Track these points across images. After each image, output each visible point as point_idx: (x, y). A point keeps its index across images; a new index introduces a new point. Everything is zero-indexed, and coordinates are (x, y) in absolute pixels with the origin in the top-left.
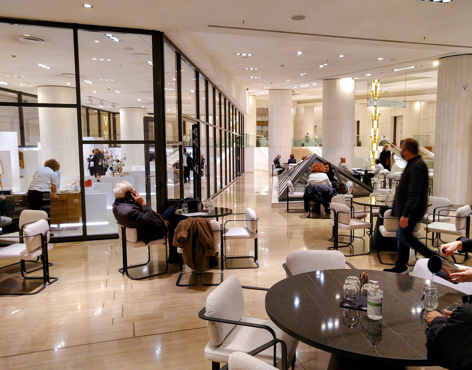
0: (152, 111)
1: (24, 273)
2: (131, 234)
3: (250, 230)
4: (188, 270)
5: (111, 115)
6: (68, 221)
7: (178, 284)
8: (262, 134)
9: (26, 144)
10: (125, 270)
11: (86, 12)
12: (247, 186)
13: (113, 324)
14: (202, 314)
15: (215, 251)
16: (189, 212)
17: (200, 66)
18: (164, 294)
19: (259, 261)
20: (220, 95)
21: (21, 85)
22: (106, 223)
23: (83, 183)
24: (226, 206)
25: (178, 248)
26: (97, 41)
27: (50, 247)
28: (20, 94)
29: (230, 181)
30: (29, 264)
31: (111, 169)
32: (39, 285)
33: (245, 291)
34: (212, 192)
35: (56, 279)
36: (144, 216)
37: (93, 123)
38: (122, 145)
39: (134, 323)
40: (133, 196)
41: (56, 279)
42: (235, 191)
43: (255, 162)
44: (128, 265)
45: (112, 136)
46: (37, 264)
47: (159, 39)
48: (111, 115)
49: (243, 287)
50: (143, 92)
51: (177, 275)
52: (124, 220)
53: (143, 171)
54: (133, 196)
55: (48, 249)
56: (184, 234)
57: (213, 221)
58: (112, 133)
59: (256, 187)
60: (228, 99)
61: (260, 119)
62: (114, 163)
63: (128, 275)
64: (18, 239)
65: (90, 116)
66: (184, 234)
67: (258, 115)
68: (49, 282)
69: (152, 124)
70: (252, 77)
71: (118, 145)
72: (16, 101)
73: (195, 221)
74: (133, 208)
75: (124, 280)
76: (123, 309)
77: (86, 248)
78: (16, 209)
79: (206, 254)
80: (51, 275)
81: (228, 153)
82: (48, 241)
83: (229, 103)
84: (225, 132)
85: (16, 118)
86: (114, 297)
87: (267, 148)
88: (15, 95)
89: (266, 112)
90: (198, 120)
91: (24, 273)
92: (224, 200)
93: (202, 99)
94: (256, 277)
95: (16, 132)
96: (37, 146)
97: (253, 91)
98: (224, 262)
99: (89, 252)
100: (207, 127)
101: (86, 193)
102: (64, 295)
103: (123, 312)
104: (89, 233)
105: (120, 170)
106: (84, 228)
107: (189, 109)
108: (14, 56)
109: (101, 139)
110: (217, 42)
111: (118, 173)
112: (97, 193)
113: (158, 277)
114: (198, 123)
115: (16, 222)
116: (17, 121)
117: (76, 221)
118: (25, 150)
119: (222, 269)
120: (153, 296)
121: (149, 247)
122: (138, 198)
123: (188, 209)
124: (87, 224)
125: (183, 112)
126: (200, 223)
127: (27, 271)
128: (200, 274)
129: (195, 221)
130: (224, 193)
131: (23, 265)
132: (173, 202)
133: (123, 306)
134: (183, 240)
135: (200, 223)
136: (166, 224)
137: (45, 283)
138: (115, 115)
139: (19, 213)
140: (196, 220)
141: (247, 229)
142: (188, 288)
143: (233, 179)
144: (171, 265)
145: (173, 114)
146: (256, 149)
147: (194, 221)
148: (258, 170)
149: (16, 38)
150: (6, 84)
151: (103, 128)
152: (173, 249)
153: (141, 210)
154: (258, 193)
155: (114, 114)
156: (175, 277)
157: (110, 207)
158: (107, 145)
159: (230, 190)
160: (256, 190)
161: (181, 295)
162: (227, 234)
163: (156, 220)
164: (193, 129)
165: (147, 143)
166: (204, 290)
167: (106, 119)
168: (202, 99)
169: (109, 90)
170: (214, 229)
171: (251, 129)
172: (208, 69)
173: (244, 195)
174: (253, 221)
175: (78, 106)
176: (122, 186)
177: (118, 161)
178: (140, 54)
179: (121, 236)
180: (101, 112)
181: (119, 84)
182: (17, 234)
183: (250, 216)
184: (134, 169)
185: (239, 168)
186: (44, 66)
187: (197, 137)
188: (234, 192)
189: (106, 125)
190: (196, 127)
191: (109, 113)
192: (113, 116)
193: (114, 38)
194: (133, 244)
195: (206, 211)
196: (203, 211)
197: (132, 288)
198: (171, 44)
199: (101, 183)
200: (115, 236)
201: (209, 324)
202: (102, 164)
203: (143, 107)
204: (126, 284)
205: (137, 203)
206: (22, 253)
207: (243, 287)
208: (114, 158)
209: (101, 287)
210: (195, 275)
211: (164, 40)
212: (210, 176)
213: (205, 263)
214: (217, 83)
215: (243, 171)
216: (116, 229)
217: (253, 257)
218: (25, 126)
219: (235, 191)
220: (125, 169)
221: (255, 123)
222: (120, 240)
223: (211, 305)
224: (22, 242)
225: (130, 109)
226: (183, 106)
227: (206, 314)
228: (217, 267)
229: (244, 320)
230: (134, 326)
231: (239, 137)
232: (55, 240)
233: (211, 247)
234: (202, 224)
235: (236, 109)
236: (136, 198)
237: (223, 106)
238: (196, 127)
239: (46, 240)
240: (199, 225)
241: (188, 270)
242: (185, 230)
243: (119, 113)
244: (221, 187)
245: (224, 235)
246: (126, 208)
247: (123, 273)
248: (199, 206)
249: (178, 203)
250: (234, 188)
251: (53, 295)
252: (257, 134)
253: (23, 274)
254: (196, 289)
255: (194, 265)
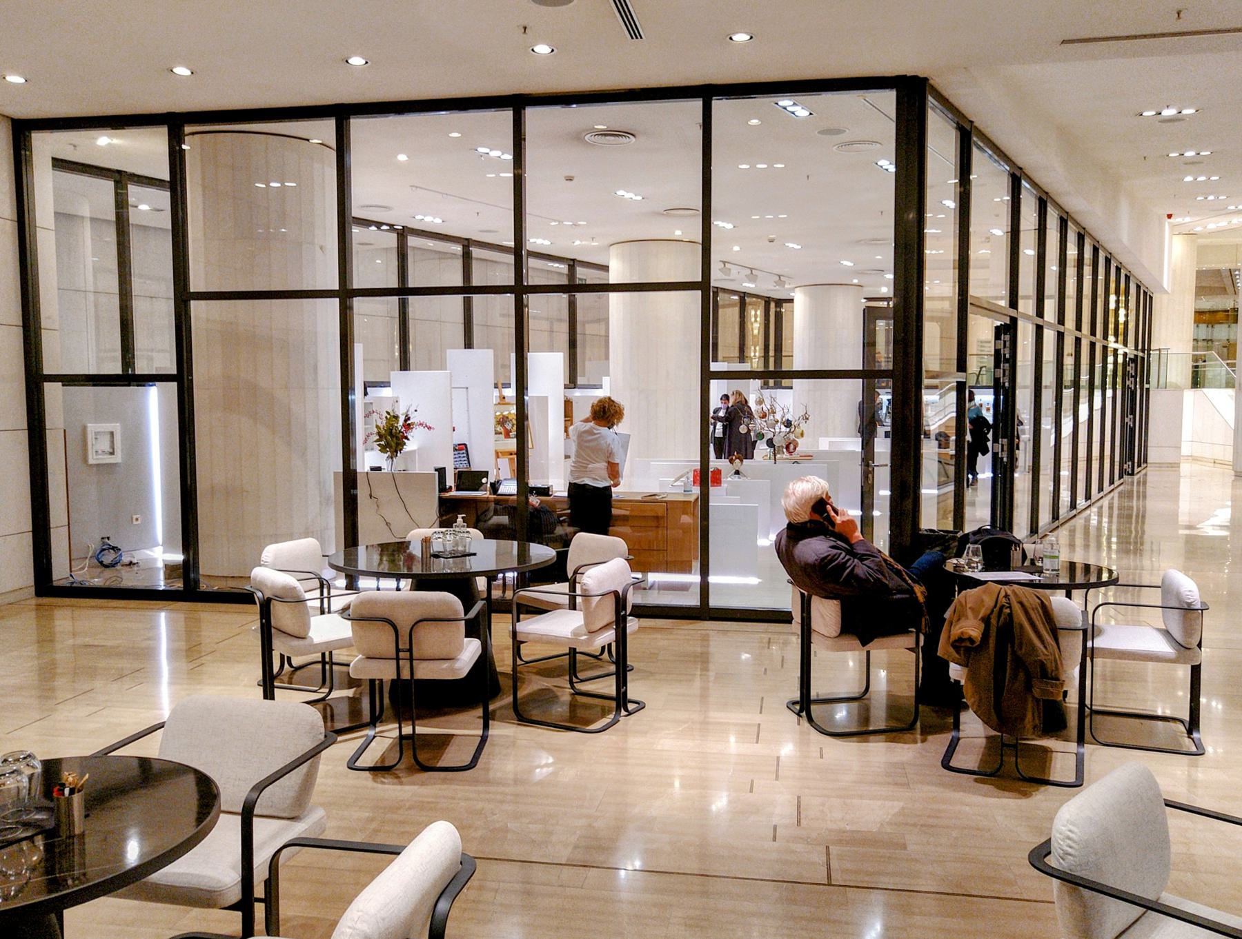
0: (886, 290)
1: (575, 680)
2: (826, 614)
3: (1177, 634)
4: (973, 727)
5: (773, 305)
6: (668, 567)
7: (946, 764)
8: (1209, 349)
9: (580, 381)
10: (804, 705)
11: (357, 76)
12: (1154, 505)
13: (774, 840)
14: (1039, 856)
15: (1062, 685)
16: (987, 568)
17: (1028, 157)
18: (907, 785)
19: (1203, 735)
20: (1081, 238)
21: (577, 243)
22: (754, 581)
23: (706, 478)
24: (1099, 559)
25: (952, 665)
26: (754, 122)
27: (633, 624)
28: (572, 264)
29: (1101, 489)
30: (584, 662)
31: (770, 443)
32: (604, 713)
33: (1176, 820)
34: (1045, 517)
35: (641, 706)
36: (861, 569)
37: (736, 330)
38: (796, 382)
39: (827, 848)
40: (832, 513)
41: (641, 706)
42: (1115, 519)
43: (1186, 434)
44: (813, 695)
45: (772, 360)
46: (599, 663)
47: (912, 95)
48: (773, 305)
49: (1169, 804)
50: (858, 242)
51: (947, 737)
52: (813, 578)
53: (853, 452)
54: (832, 513)
55: (628, 631)
56: (972, 628)
57: (1057, 599)
58: (772, 353)
59: (1185, 508)
60: (1105, 250)
61: (1207, 304)
62: (777, 430)
63: (810, 720)
64: (565, 600)
65: (720, 311)
66: (972, 628)
67: (1201, 291)
68: (626, 710)
69: (883, 328)
70: (1189, 179)
71: (785, 382)
72: (564, 281)
73: (1006, 596)
74: (833, 547)
75: (802, 733)
76: (799, 807)
77: (705, 639)
78: (560, 531)
79: (1036, 692)
80: (630, 696)
81: (1097, 408)
82: (629, 610)
83: (1108, 261)
84: (1093, 345)
85: (560, 320)
86: (777, 771)
87: (1231, 392)
88: (563, 268)
89: (1228, 281)
90: (1012, 312)
91: (575, 680)
92: (1079, 541)
93: (1028, 252)
94: (1192, 783)
95: (561, 354)
96: (600, 387)
97: (1187, 219)
98: (1087, 721)
99: (712, 649)
100: (1039, 330)
101: (712, 503)
102: (659, 747)
103: (799, 813)
104: (714, 602)
105: (792, 447)
106: (705, 588)
107: (988, 281)
108: (570, 179)
109: (745, 367)
110: (1073, 83)
111: (786, 455)
112: (733, 502)
113: (882, 737)
114: (1014, 321)
115: (562, 557)
116: (565, 327)
117: (685, 568)
118: (577, 393)
119: (1081, 741)
120: (875, 787)
121: (868, 653)
122: (845, 519)
123: (984, 558)
124: (712, 579)
125: (974, 291)
126: (1021, 603)
127: (581, 675)
128: (1015, 746)
129: (1006, 596)
130: (1079, 522)
131: (572, 662)
132: (934, 538)
133: (799, 797)
134: (968, 644)
135: (1021, 603)
136: (919, 594)
137: (618, 709)
138: (781, 307)
139: (566, 542)
140: (1009, 592)
141: (1167, 633)
142: (976, 780)
143: (1112, 482)
144: (932, 706)
145: (942, 299)
146: (1190, 395)
147: (1003, 593)
148: (1195, 459)
149: (578, 138)
150: (547, 243)
151: (749, 340)
152: (932, 669)
153: (851, 552)
154: (1190, 527)
155: (779, 303)
156: (939, 743)
157: (767, 540)
158: (758, 382)
159: (1098, 516)
160: (1183, 519)
161: (958, 795)
162: (1099, 643)
163: (892, 581)
164: (997, 337)
165: (869, 375)
166: (1025, 795)
167: (756, 316)
168: (1028, 252)
169: (771, 241)
170: (1061, 623)
171: (1174, 336)
172: (1049, 168)
173: (1143, 532)
174: (1189, 612)
175: (703, 285)
176: (807, 486)
177: (788, 424)
178: (859, 142)
179: (797, 617)
180: (748, 300)
181: (809, 226)
182: (564, 587)
183: (1178, 596)
184: (824, 444)
185: (1132, 451)
186: (628, 195)
187: (1006, 361)
188: (1110, 522)
189: (756, 332)
190: (1007, 331)
191: (768, 301)
192: (776, 308)
193: (795, 107)
194: (829, 642)
195: (1034, 568)
196: (1022, 569)
197: (822, 757)
198: (947, 105)
199: (743, 479)
200: (783, 617)
201: (1060, 891)
202: (749, 431)
203: (855, 281)
204: (803, 743)
205: (840, 535)
206: (576, 633)
207: (1169, 804)
208: (778, 417)
209: (728, 742)
210: (995, 748)
211: (930, 100)
212: (1041, 472)
213: (1029, 715)
214: (1075, 203)
215: (1144, 460)
216: (785, 597)
217: (1182, 721)
218: (579, 337)
219: (1115, 519)
220: (803, 446)
221: (1190, 317)
222: (796, 626)
223: (1069, 838)
224: (573, 606)
225: (820, 288)
226: (974, 274)
227: (1052, 861)
228: (1064, 733)
229: (1169, 899)
230: (828, 854)
231: (1134, 360)
232: (642, 612)
233: (1049, 674)
234: (1027, 604)
235: (1127, 278)
236: (839, 519)
237: (1087, 270)
238: (1007, 331)
239: (625, 608)
240: (1017, 608)
241: (973, 727)
242: (976, 617)
243: (791, 301)
244: (1073, 505)
245: (1089, 644)
246: (814, 548)
247: (798, 715)
248: (1016, 555)
249: (953, 542)
250: (1111, 508)
251: (634, 742)
252: (1195, 349)
253: (571, 683)
254: (998, 787)
255: (1001, 717)
